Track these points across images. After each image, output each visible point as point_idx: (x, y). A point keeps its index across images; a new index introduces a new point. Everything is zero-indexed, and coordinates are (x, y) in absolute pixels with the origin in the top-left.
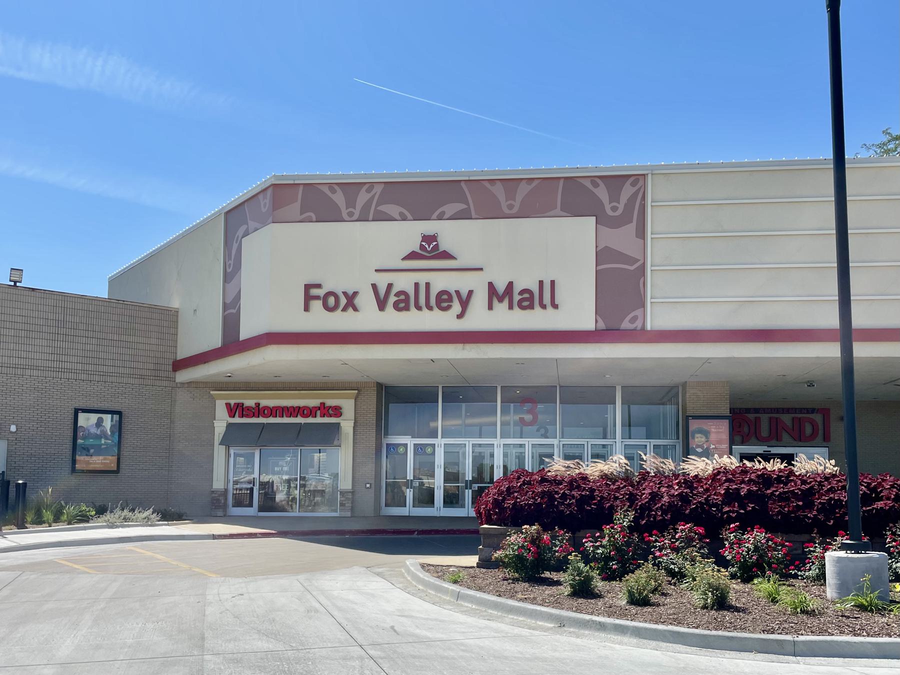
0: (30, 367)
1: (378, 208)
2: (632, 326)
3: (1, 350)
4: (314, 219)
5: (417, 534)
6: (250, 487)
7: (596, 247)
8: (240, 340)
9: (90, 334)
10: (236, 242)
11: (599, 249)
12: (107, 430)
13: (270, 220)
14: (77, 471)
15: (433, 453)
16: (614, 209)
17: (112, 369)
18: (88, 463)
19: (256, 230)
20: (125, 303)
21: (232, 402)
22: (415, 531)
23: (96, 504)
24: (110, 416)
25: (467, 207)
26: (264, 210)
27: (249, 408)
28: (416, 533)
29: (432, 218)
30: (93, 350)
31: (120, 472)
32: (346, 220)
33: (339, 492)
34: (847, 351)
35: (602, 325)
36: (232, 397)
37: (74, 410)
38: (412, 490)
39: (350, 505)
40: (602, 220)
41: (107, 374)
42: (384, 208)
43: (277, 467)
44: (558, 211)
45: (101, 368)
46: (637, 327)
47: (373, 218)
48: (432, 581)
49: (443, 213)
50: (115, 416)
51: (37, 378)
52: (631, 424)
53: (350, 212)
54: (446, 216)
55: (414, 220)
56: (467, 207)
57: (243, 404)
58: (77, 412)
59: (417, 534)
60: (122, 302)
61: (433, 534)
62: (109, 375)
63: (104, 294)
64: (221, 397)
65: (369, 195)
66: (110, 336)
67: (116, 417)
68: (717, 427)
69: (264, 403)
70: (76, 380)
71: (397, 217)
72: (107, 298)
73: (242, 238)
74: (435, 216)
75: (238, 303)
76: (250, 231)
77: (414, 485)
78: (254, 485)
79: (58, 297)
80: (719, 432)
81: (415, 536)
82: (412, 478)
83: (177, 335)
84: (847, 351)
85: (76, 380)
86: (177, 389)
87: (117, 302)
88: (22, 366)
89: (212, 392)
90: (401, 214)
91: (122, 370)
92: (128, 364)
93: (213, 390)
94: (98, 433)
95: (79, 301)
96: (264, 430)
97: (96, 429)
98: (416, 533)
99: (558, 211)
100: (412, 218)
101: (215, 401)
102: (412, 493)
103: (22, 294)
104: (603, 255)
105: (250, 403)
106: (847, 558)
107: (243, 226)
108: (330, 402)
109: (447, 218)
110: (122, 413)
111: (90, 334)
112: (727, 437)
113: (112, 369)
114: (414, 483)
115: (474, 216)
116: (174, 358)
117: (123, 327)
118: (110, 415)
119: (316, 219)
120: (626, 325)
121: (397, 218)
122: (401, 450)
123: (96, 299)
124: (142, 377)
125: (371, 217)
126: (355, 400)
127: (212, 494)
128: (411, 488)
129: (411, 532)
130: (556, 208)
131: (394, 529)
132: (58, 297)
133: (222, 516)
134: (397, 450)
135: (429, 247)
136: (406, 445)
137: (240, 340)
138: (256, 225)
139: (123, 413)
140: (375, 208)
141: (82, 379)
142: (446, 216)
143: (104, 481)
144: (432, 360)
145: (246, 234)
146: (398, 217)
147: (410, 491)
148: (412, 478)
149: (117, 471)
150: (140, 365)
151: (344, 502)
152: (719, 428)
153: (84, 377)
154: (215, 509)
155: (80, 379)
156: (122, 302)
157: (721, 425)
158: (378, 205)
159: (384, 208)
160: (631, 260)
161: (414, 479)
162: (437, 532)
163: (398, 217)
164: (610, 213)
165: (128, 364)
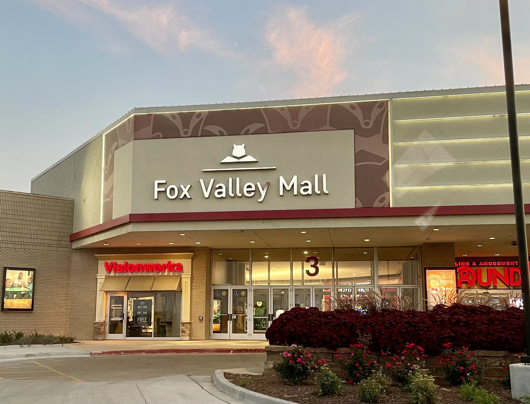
0: (16, 242)
1: (204, 128)
2: (381, 205)
3: (1, 232)
4: (161, 136)
5: (233, 352)
6: (120, 320)
7: (355, 150)
8: (113, 219)
9: (16, 217)
10: (111, 154)
11: (356, 151)
12: (25, 282)
13: (133, 138)
14: (4, 309)
15: (246, 296)
16: (367, 124)
17: (29, 240)
18: (12, 304)
19: (123, 145)
20: (39, 196)
21: (109, 262)
22: (231, 350)
23: (16, 331)
24: (27, 272)
25: (265, 125)
26: (128, 132)
27: (120, 266)
28: (232, 351)
29: (241, 134)
30: (17, 228)
31: (34, 310)
32: (183, 136)
33: (181, 323)
34: (520, 220)
35: (360, 205)
36: (109, 258)
37: (4, 268)
38: (232, 321)
39: (189, 332)
40: (359, 132)
41: (23, 243)
42: (207, 128)
43: (139, 306)
44: (327, 126)
45: (22, 240)
46: (384, 205)
47: (201, 135)
48: (445, 389)
49: (249, 130)
50: (31, 272)
51: (33, 250)
52: (387, 274)
53: (185, 131)
54: (250, 132)
55: (229, 135)
56: (265, 125)
57: (116, 263)
58: (5, 269)
59: (233, 352)
60: (37, 195)
61: (243, 352)
62: (54, 246)
63: (27, 190)
64: (102, 259)
65: (198, 120)
66: (28, 218)
67: (32, 273)
68: (447, 275)
69: (130, 262)
70: (6, 248)
71: (218, 134)
72: (30, 193)
73: (115, 150)
74: (242, 132)
75: (112, 194)
76: (119, 146)
77: (233, 318)
78: (123, 318)
79: (5, 194)
80: (448, 279)
81: (231, 353)
82: (231, 313)
83: (73, 217)
84: (520, 220)
85: (6, 248)
86: (73, 253)
87: (34, 195)
88: (16, 242)
89: (95, 255)
90: (220, 131)
91: (36, 241)
92: (40, 237)
93: (96, 254)
94: (20, 284)
95: (38, 199)
96: (130, 280)
97: (18, 281)
98: (232, 351)
99: (327, 126)
100: (227, 134)
101: (98, 261)
102: (231, 323)
103: (21, 197)
104: (359, 156)
105: (121, 262)
106: (525, 368)
107: (115, 143)
108: (175, 261)
109: (251, 133)
110: (35, 270)
111: (16, 217)
112: (454, 282)
113: (29, 240)
114: (233, 316)
115: (269, 131)
116: (71, 232)
117: (37, 212)
118: (28, 271)
119: (163, 136)
120: (377, 204)
121: (217, 134)
122: (224, 293)
123: (20, 194)
124: (49, 246)
125: (199, 135)
126: (192, 259)
127: (95, 324)
128: (231, 320)
129: (228, 351)
130: (379, 133)
131: (216, 349)
132: (5, 194)
133: (102, 340)
134: (221, 293)
135: (239, 153)
136: (227, 290)
137: (113, 219)
138: (125, 142)
139: (36, 269)
140: (203, 128)
141: (10, 247)
142: (250, 132)
143: (23, 317)
144: (242, 231)
145: (117, 148)
146: (218, 134)
147: (230, 322)
148: (231, 313)
149: (32, 309)
150: (48, 237)
151: (184, 330)
152: (448, 276)
153: (11, 246)
154: (97, 335)
155: (18, 248)
156: (37, 195)
157: (450, 274)
158: (205, 125)
159: (207, 128)
160: (380, 159)
161: (233, 314)
162: (246, 351)
163: (218, 134)
164: (364, 126)
165: (40, 237)
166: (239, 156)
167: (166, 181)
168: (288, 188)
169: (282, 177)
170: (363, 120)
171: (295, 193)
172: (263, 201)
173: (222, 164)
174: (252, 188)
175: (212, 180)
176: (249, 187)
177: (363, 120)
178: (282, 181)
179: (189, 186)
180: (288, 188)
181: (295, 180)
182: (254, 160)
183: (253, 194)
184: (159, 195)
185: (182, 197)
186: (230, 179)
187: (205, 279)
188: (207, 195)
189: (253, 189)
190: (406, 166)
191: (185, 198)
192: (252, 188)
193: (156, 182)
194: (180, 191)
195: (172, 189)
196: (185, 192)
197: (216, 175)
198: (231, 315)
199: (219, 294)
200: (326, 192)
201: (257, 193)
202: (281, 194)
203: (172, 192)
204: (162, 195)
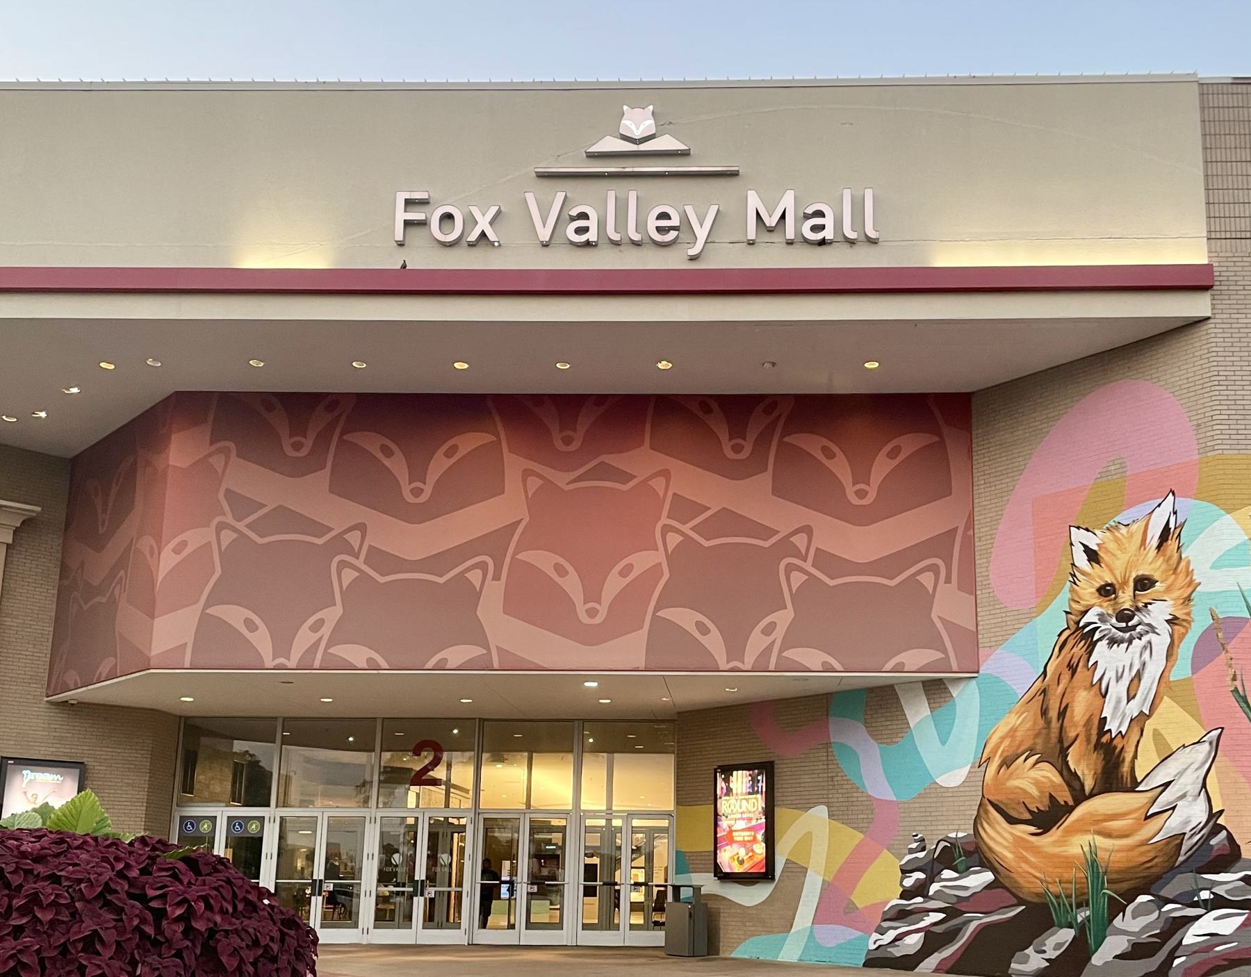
77: (324, 888)
128: (320, 895)
148: (322, 877)
166: (637, 134)
167: (429, 196)
168: (771, 221)
169: (753, 192)
170: (584, 604)
171: (790, 234)
172: (702, 251)
173: (541, 180)
174: (670, 219)
175: (560, 197)
176: (664, 216)
177: (584, 604)
178: (754, 201)
179: (493, 210)
180: (771, 221)
181: (788, 201)
182: (679, 146)
183: (673, 234)
184: (407, 231)
185: (473, 236)
186: (611, 196)
187: (145, 804)
188: (545, 234)
189: (675, 221)
190: (1204, 941)
191: (483, 242)
192: (670, 219)
193: (401, 198)
194: (471, 221)
195: (448, 217)
196: (483, 224)
197: (569, 185)
198: (321, 881)
199: (241, 828)
200: (872, 234)
201: (684, 237)
202: (752, 235)
203: (447, 223)
204: (416, 234)
